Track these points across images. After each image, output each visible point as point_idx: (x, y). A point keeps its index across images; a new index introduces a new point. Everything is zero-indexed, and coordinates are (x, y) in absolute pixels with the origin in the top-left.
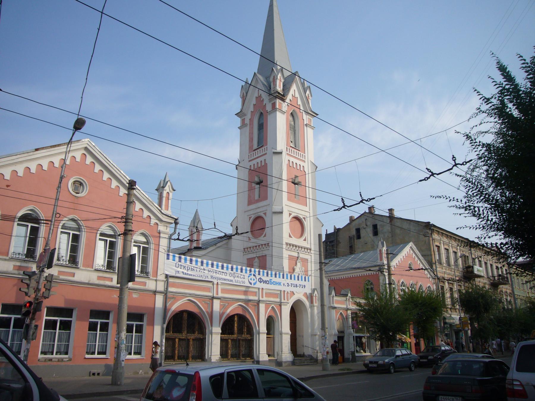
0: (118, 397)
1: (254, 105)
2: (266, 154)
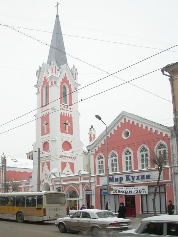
0: (167, 209)
2: (49, 109)
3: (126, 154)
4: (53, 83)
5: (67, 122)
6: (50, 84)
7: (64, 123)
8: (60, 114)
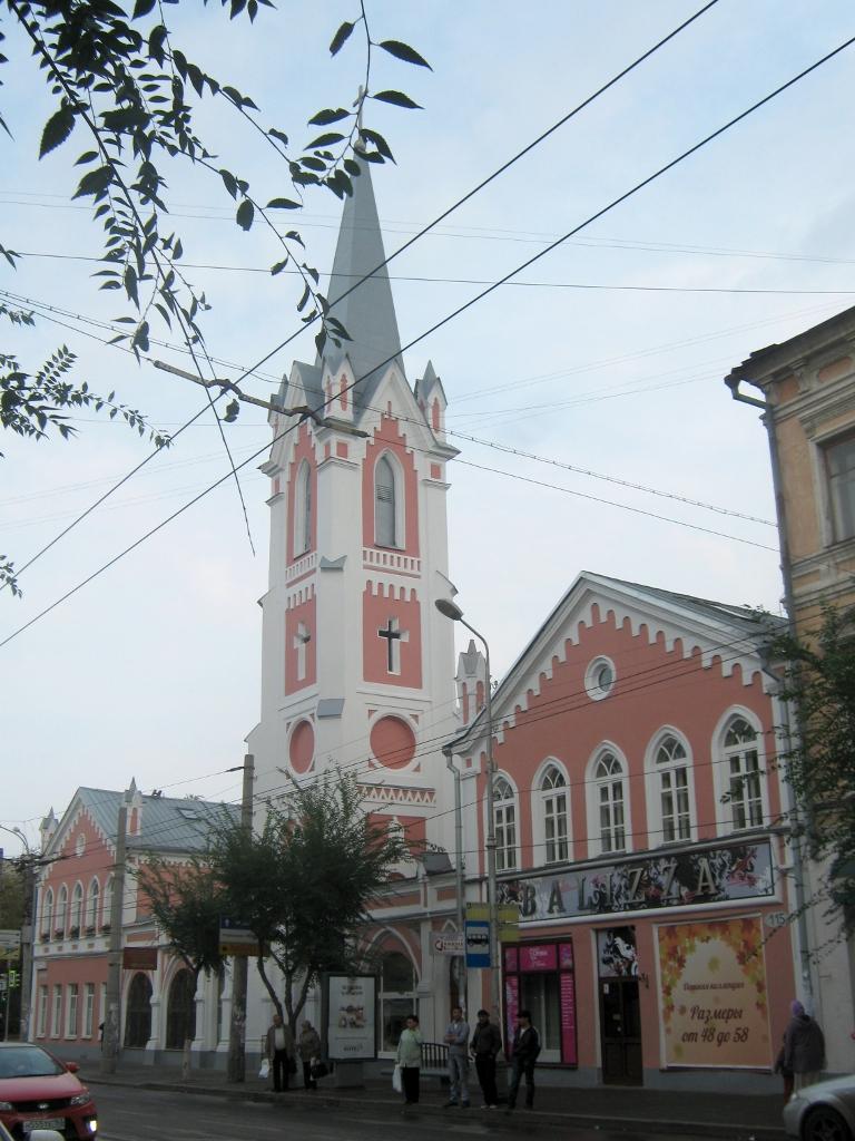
1: (296, 445)
3: (662, 757)
4: (334, 452)
5: (395, 628)
6: (319, 457)
7: (382, 633)
8: (365, 588)
